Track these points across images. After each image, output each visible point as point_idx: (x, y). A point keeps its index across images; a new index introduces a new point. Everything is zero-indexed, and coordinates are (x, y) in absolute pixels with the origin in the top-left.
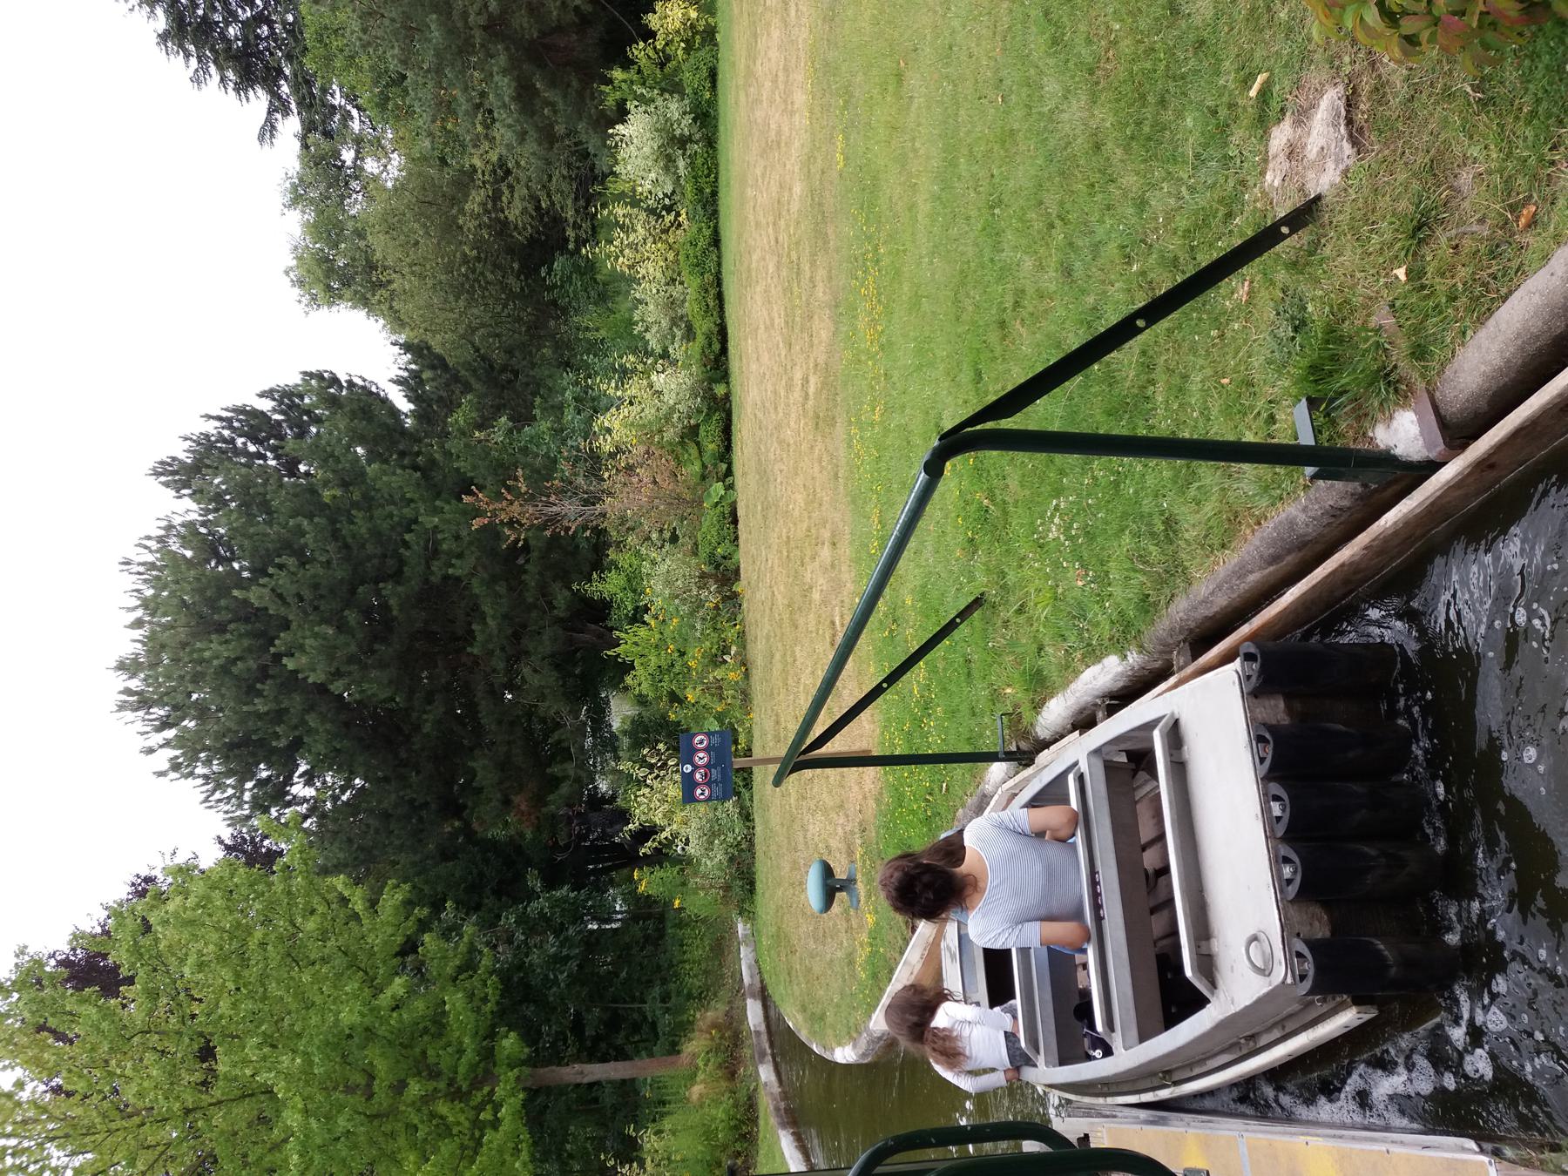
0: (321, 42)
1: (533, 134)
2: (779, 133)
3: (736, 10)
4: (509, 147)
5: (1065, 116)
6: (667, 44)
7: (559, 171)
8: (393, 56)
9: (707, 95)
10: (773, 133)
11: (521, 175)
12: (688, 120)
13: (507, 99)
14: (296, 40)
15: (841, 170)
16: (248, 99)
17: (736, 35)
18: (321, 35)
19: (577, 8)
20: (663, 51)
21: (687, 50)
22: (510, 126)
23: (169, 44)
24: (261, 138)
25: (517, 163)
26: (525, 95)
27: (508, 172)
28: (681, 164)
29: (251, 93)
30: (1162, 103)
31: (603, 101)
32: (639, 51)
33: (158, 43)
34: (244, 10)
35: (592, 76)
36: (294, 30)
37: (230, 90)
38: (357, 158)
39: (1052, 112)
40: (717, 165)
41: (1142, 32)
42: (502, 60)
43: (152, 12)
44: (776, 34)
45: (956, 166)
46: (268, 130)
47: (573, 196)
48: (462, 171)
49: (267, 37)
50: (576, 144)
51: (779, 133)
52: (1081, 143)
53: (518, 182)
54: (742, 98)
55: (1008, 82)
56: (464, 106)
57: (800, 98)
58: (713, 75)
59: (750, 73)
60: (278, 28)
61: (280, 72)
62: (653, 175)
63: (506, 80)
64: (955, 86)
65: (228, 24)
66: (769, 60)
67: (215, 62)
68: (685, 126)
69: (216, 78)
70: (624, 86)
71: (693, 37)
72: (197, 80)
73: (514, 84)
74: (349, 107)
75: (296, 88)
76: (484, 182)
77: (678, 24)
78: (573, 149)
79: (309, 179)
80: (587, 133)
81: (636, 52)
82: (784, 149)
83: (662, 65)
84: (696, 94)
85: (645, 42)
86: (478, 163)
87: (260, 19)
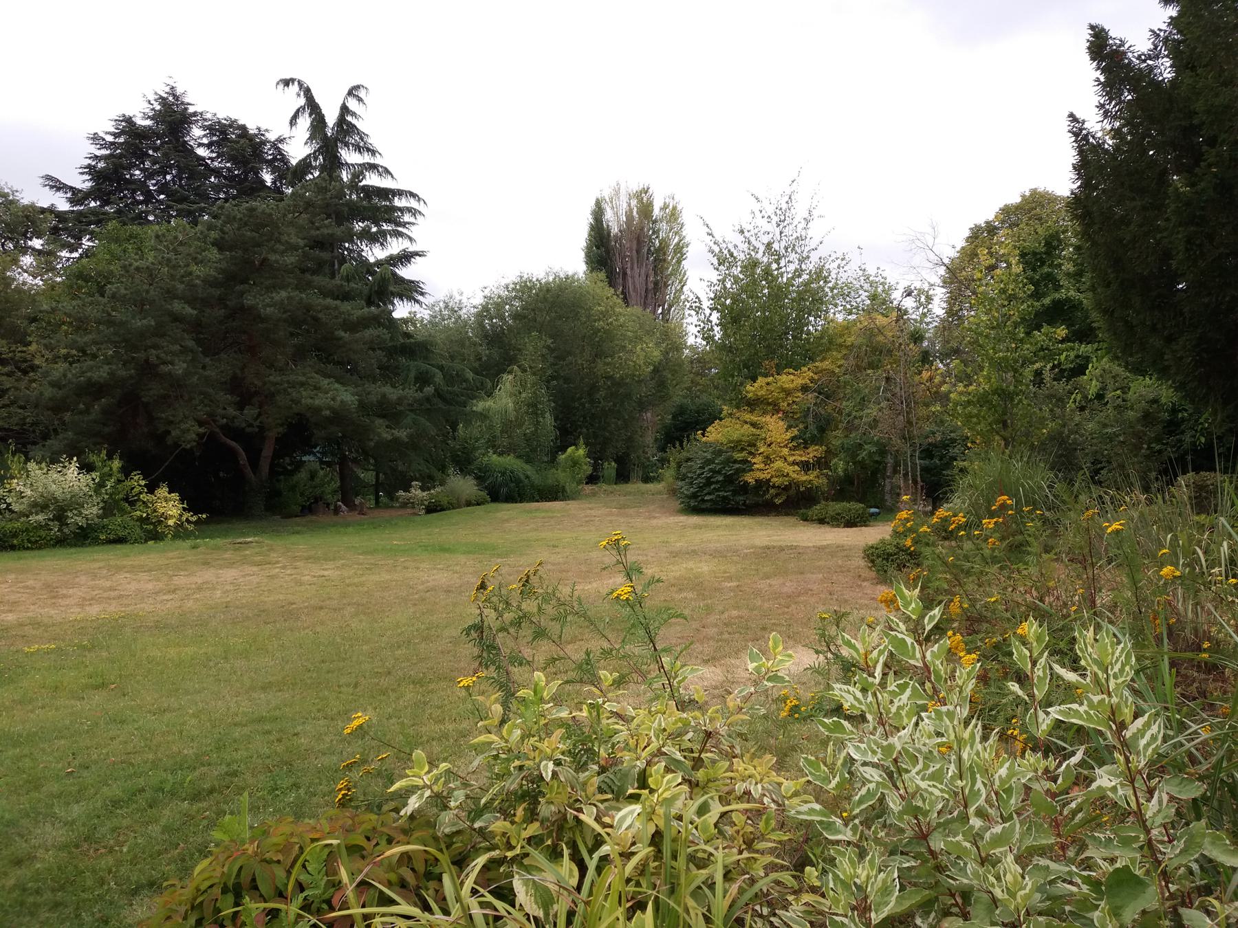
0: (131, 236)
1: (60, 394)
2: (65, 596)
3: (171, 555)
4: (46, 374)
5: (48, 828)
6: (144, 502)
7: (29, 416)
8: (118, 288)
9: (103, 537)
10: (65, 592)
11: (23, 385)
12: (81, 521)
13: (89, 374)
14: (133, 219)
15: (23, 651)
16: (82, 173)
17: (152, 556)
18: (136, 238)
19: (169, 432)
20: (138, 500)
21: (140, 519)
22: (65, 375)
23: (123, 124)
24: (49, 178)
25: (34, 381)
26: (94, 390)
27: (25, 372)
28: (40, 517)
29: (88, 177)
30: (56, 905)
31: (93, 452)
32: (137, 481)
33: (124, 116)
34: (154, 185)
35: (116, 443)
36: (141, 219)
37: (89, 161)
38: (34, 249)
39: (54, 815)
40: (40, 548)
41: (117, 871)
42: (122, 373)
43: (149, 117)
44: (150, 586)
45: (14, 746)
46: (57, 185)
47: (7, 427)
48: (26, 334)
49: (134, 198)
50: (55, 430)
51: (65, 596)
52: (21, 847)
53: (16, 380)
54: (97, 565)
55: (85, 774)
56: (83, 339)
57: (94, 610)
58: (120, 540)
59: (119, 569)
60: (142, 207)
61: (106, 202)
62: (29, 492)
63: (105, 375)
64: (88, 732)
65: (143, 170)
66: (129, 583)
67: (111, 155)
68: (74, 519)
69: (99, 153)
70: (107, 469)
71: (152, 523)
72: (95, 138)
73: (102, 381)
74: (80, 251)
75: (93, 212)
76: (14, 351)
77: (161, 510)
78: (51, 428)
79: (13, 210)
80: (64, 438)
81: (136, 478)
82: (49, 602)
83: (126, 500)
84: (103, 527)
85: (145, 485)
86: (33, 348)
87: (149, 196)
